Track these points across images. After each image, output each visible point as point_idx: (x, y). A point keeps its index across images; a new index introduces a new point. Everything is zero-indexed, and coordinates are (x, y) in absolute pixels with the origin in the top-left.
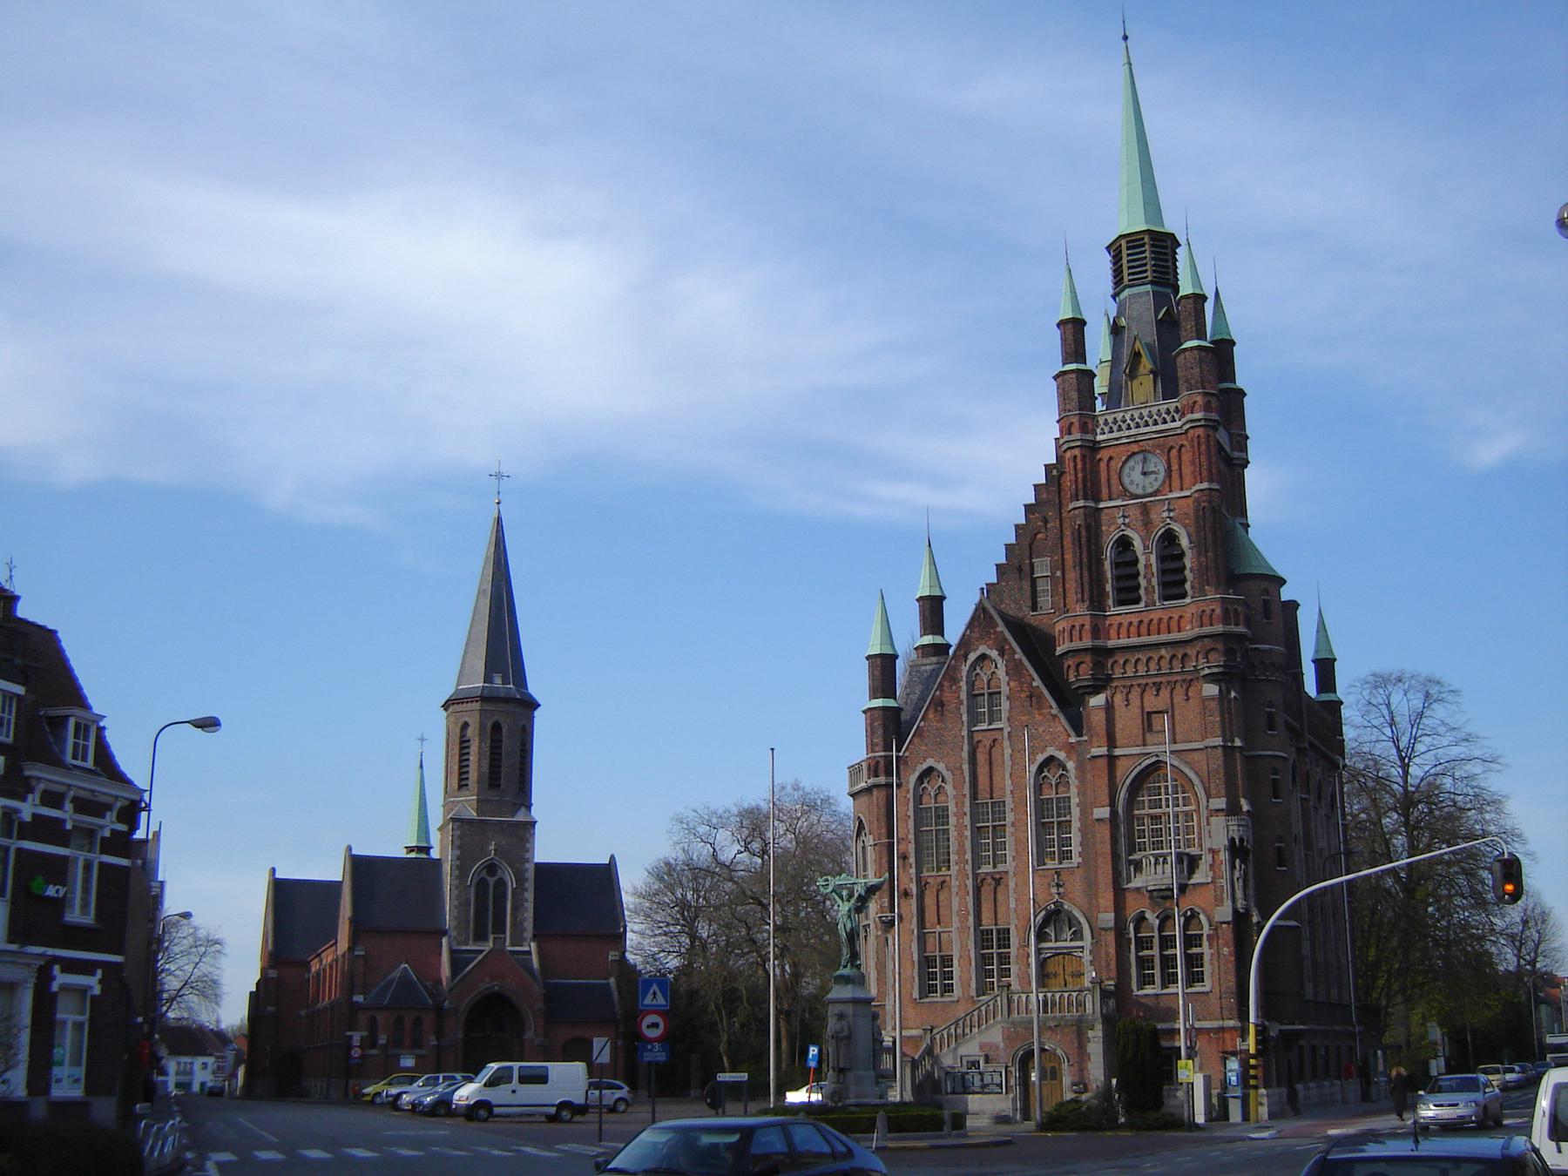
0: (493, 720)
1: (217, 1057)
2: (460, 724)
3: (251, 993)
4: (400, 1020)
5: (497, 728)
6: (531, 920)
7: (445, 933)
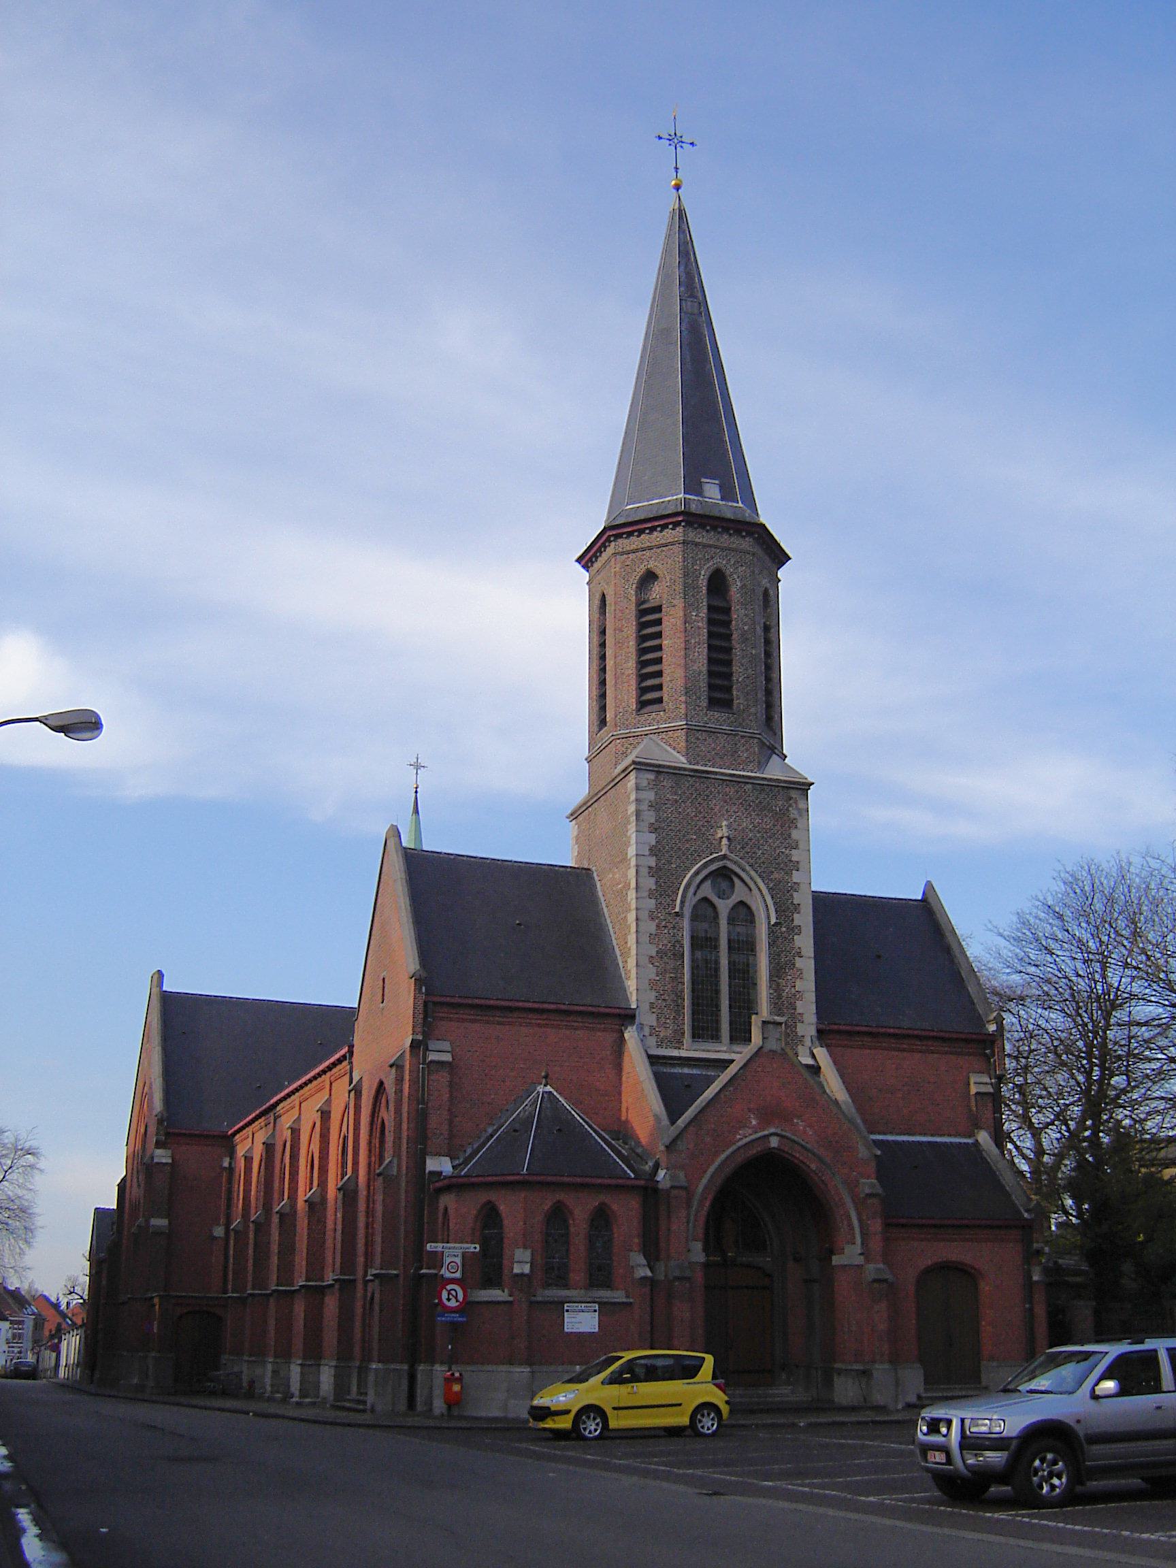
1: (12, 1322)
2: (635, 578)
3: (99, 1212)
4: (558, 1215)
5: (718, 583)
6: (811, 997)
7: (629, 1017)
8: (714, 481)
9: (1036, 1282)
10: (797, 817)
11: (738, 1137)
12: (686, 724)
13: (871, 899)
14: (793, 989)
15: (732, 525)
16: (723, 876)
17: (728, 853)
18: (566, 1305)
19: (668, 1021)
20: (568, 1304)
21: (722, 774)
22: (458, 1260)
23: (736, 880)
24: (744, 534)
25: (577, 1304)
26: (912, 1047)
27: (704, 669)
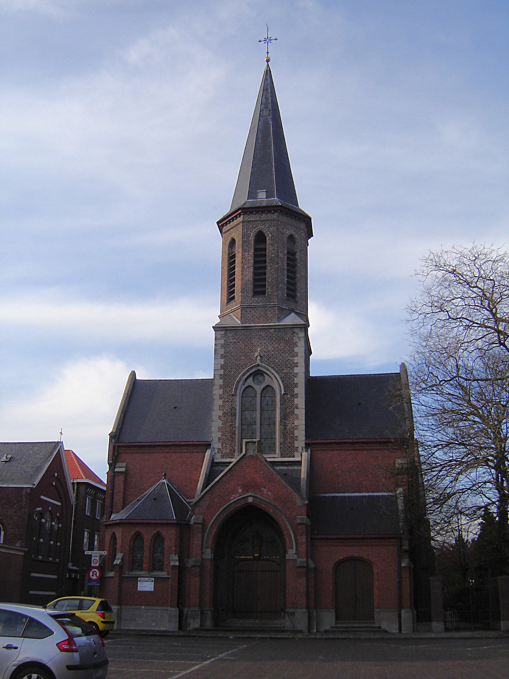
0: (256, 230)
4: (138, 536)
8: (263, 191)
9: (403, 567)
10: (297, 341)
11: (232, 498)
12: (240, 306)
13: (369, 376)
14: (293, 425)
15: (271, 209)
16: (258, 374)
17: (260, 363)
18: (139, 579)
19: (227, 446)
20: (140, 578)
21: (258, 326)
22: (98, 558)
23: (265, 375)
24: (273, 212)
25: (144, 578)
26: (355, 448)
27: (251, 279)
